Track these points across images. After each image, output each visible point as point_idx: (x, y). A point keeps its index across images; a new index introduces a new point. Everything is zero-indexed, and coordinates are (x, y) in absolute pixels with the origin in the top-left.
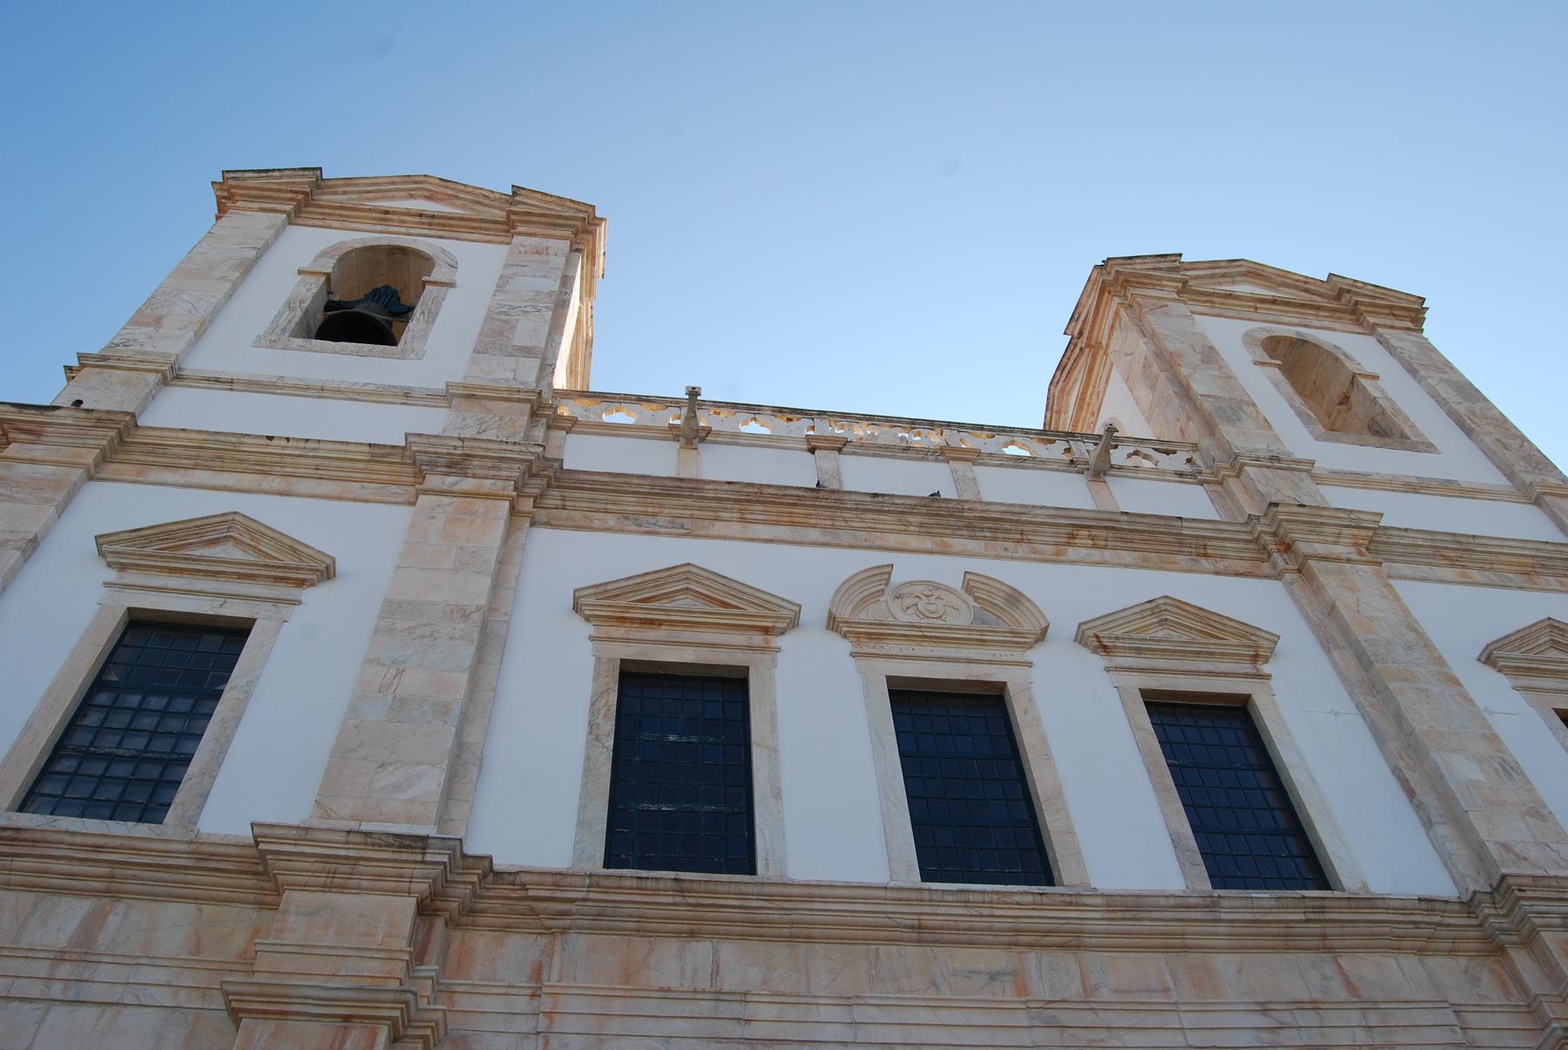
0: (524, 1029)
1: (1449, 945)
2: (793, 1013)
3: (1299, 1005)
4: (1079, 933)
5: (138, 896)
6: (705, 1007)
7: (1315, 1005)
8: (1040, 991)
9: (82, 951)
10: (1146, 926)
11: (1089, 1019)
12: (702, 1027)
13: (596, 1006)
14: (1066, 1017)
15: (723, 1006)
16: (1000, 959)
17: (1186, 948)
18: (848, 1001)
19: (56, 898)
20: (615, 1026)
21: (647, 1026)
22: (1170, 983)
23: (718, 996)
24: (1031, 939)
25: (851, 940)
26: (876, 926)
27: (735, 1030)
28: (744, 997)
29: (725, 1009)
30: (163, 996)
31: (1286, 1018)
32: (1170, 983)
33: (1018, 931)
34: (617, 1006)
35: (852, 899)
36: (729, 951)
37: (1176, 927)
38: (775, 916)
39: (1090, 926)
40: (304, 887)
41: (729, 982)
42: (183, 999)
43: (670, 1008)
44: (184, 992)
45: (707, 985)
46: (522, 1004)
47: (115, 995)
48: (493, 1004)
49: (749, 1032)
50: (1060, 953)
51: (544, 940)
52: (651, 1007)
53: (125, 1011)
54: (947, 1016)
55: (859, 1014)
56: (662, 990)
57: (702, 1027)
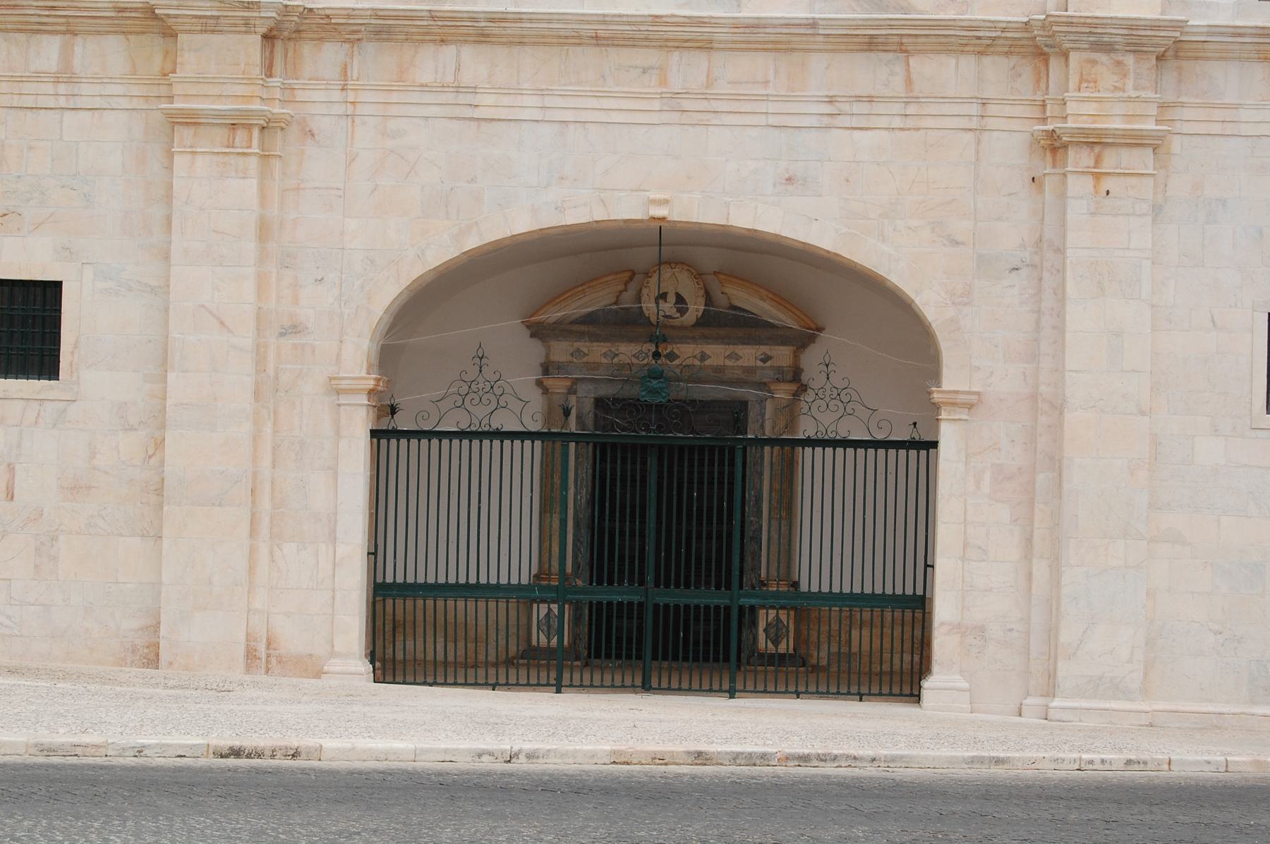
0: (340, 112)
1: (1006, 49)
2: (506, 100)
3: (858, 99)
4: (711, 42)
5: (89, 33)
6: (449, 97)
7: (871, 99)
8: (676, 84)
9: (65, 75)
10: (760, 37)
11: (703, 105)
12: (449, 111)
13: (381, 97)
14: (686, 105)
15: (461, 96)
16: (651, 57)
17: (793, 50)
18: (541, 93)
19: (38, 36)
20: (394, 110)
21: (413, 111)
22: (772, 78)
23: (458, 89)
24: (676, 44)
25: (550, 44)
26: (566, 37)
27: (468, 112)
28: (474, 90)
29: (463, 99)
30: (124, 103)
31: (846, 107)
32: (772, 78)
33: (667, 40)
34: (395, 97)
35: (550, 21)
36: (468, 51)
37: (784, 38)
38: (496, 31)
39: (717, 37)
40: (189, 32)
41: (466, 79)
42: (136, 103)
43: (428, 98)
44: (135, 99)
45: (450, 79)
46: (337, 96)
47: (98, 103)
48: (318, 96)
49: (477, 113)
50: (697, 52)
51: (347, 46)
52: (415, 97)
53: (105, 113)
54: (606, 103)
55: (549, 101)
56: (422, 86)
57: (449, 111)
